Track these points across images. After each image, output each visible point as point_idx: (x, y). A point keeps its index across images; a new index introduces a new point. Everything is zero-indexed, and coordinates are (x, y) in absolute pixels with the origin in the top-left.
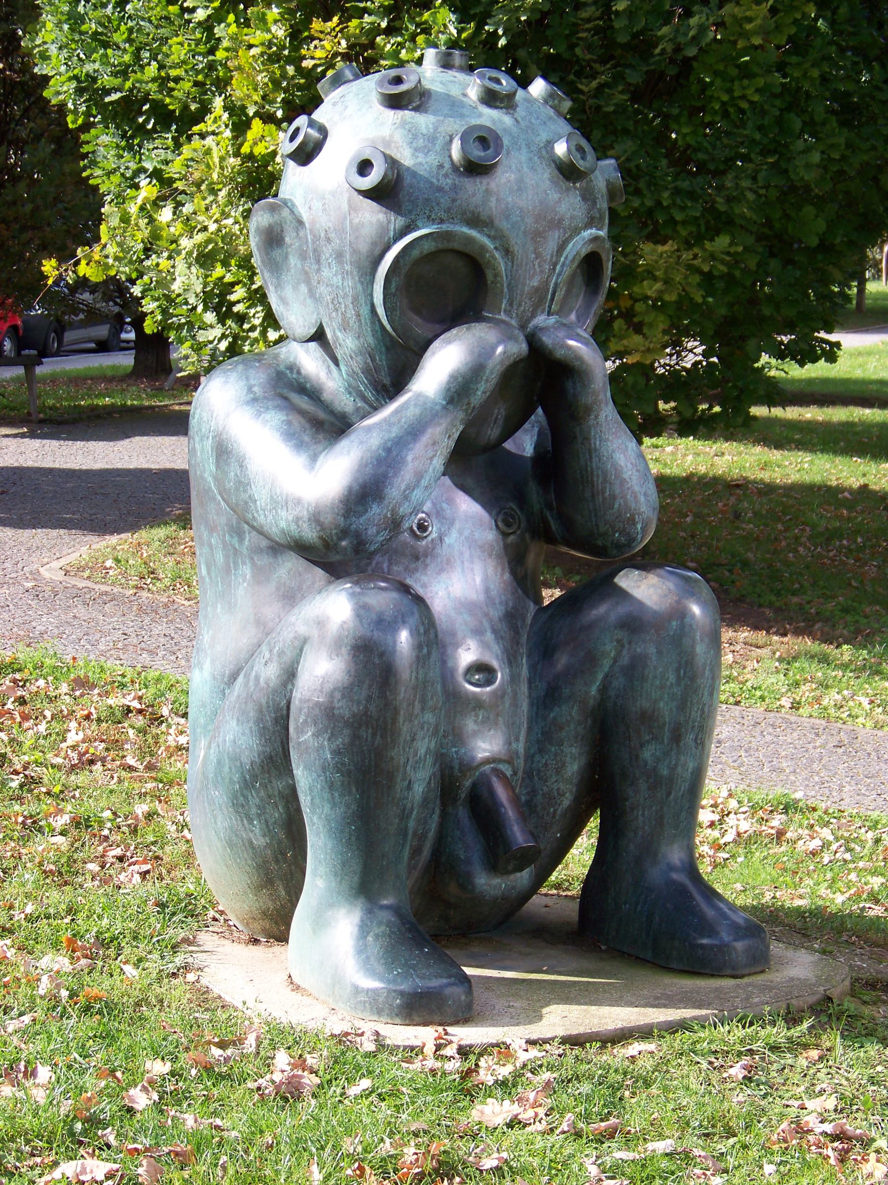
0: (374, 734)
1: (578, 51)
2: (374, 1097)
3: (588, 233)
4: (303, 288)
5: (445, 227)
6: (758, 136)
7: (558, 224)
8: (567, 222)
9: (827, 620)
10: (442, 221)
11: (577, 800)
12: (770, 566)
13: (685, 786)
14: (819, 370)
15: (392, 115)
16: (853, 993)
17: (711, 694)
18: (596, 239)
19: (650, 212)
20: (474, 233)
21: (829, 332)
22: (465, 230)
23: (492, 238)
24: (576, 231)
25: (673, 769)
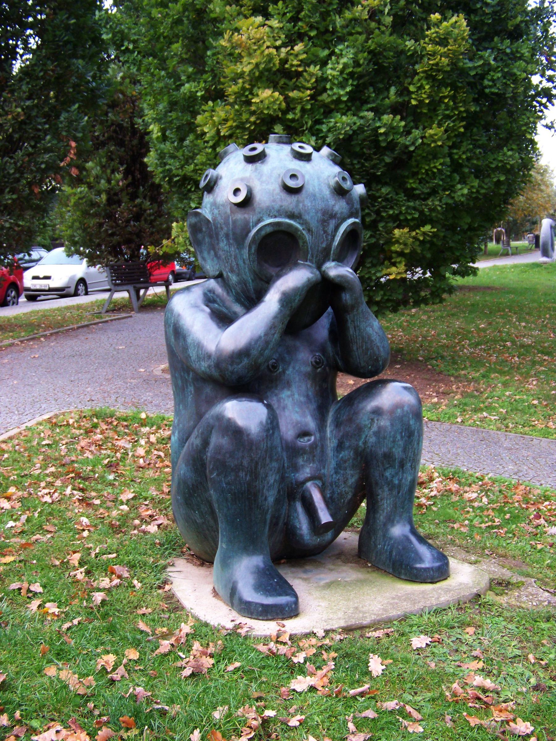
0: (246, 475)
1: (365, 150)
2: (240, 672)
3: (351, 221)
4: (212, 252)
5: (277, 220)
6: (441, 183)
7: (333, 216)
8: (339, 215)
9: (476, 381)
10: (275, 217)
11: (355, 495)
12: (453, 358)
13: (406, 489)
14: (469, 280)
15: (250, 167)
16: (490, 588)
17: (418, 444)
18: (354, 223)
19: (398, 215)
20: (292, 222)
21: (474, 263)
22: (288, 221)
23: (301, 224)
24: (344, 220)
25: (400, 481)
